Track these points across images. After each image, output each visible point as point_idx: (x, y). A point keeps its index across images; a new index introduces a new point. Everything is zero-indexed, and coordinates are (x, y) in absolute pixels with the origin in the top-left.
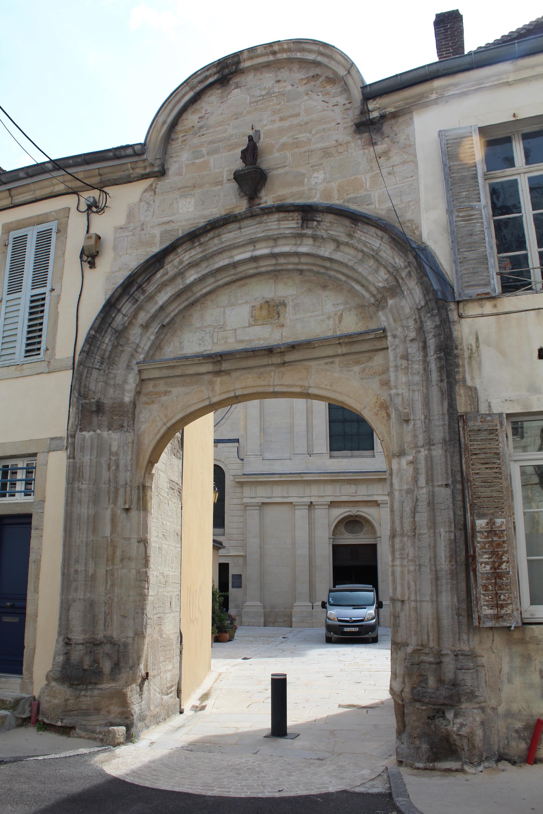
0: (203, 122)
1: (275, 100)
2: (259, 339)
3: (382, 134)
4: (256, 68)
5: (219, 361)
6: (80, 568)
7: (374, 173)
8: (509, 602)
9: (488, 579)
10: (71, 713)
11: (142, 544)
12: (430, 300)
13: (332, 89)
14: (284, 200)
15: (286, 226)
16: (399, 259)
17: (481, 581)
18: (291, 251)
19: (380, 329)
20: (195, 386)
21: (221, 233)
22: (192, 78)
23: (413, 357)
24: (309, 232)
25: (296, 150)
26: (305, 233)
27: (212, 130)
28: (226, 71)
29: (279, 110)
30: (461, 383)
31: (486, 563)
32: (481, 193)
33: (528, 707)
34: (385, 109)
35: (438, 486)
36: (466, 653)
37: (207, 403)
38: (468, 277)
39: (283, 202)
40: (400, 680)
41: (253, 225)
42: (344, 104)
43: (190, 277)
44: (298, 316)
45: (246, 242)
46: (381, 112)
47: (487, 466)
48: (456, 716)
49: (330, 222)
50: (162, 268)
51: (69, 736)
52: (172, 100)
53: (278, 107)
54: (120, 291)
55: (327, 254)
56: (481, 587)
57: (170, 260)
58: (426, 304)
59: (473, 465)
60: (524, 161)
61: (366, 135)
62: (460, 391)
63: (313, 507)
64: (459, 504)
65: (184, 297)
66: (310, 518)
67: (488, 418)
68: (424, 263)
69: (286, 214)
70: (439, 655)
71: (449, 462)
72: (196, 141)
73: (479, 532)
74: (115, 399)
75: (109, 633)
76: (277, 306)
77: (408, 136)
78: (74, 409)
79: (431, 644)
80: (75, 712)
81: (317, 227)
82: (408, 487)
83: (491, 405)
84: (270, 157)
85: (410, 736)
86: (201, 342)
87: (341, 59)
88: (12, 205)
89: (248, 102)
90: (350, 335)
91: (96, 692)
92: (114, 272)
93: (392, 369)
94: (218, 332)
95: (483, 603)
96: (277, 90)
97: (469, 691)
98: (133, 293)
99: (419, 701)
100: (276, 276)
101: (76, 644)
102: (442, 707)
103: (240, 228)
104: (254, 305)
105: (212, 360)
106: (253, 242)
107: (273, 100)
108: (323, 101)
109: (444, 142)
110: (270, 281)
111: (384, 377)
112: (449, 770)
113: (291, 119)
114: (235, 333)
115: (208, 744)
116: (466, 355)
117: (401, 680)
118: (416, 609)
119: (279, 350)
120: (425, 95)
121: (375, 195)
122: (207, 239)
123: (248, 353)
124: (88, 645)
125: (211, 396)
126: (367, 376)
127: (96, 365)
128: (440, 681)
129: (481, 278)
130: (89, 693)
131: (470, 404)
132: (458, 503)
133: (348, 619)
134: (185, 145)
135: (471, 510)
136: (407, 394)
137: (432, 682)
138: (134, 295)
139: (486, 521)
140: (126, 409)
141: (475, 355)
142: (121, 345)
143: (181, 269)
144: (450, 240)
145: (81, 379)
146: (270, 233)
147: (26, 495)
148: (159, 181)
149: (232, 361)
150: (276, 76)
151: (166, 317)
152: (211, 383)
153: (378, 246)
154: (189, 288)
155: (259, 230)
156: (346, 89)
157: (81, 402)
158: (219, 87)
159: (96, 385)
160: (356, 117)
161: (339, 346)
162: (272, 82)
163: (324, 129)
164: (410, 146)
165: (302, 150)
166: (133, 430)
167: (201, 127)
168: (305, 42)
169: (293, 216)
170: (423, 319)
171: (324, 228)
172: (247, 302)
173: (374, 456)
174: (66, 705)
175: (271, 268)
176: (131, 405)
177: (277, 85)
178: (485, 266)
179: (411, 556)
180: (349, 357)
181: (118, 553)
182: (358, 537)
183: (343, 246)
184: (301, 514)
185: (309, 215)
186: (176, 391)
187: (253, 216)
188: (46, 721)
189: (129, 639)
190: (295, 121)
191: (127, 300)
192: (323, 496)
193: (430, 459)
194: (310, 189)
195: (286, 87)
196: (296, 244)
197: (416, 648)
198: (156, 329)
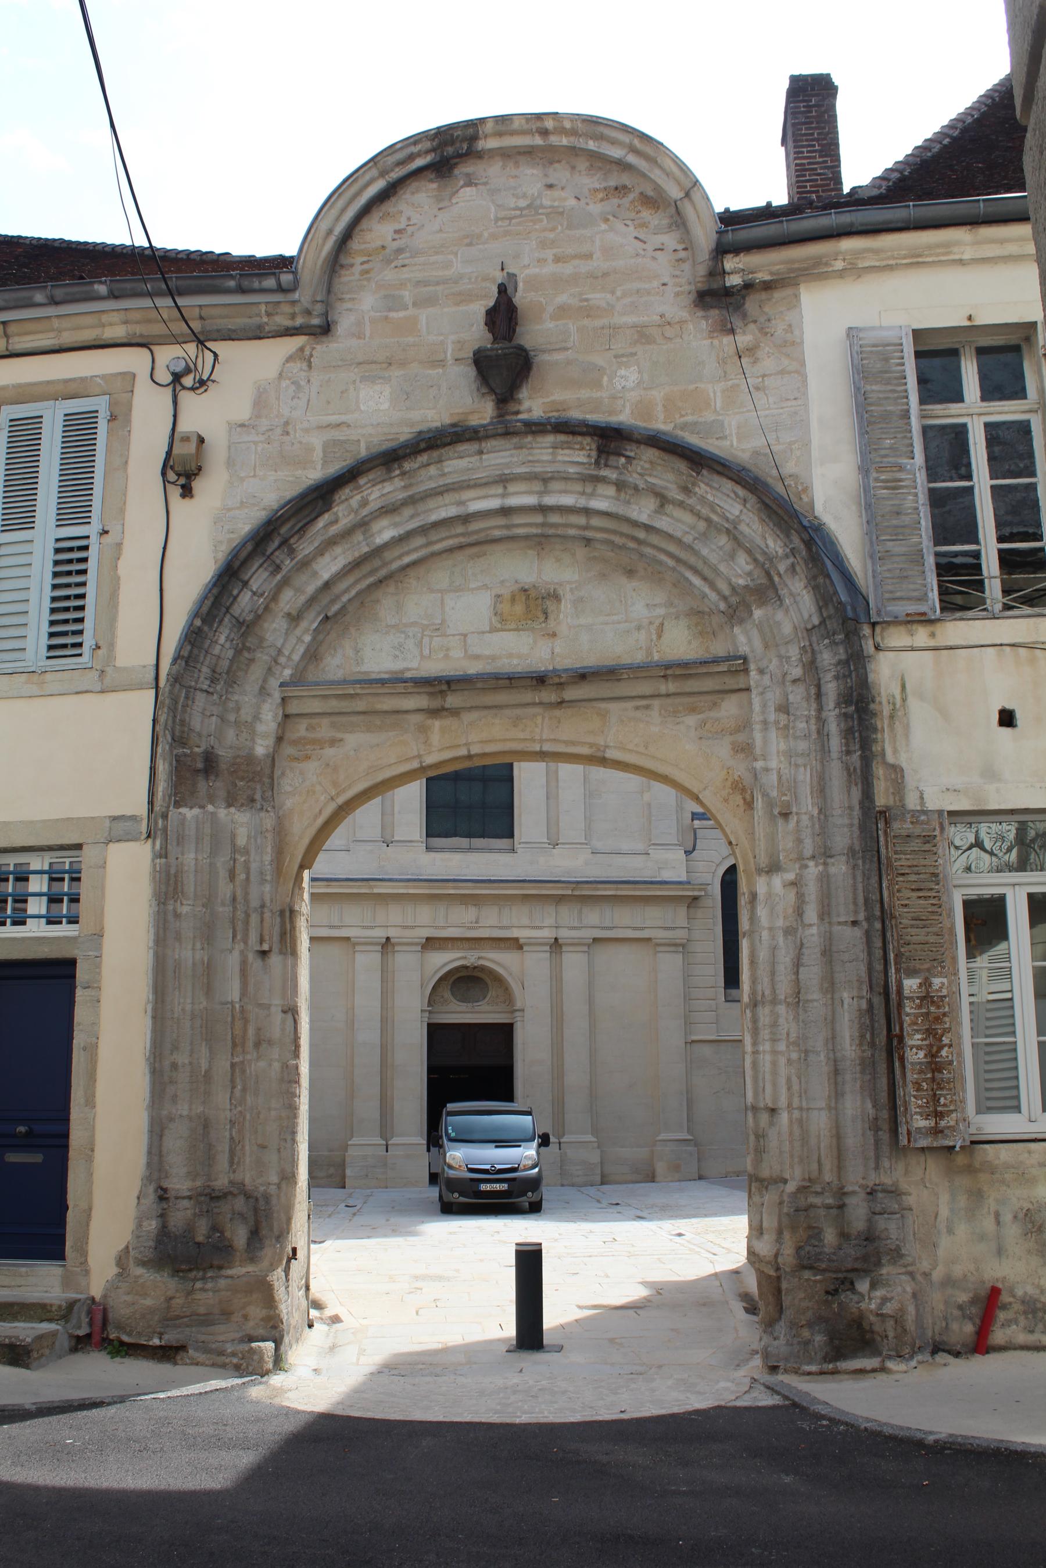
0: (403, 241)
1: (545, 221)
2: (510, 656)
3: (744, 316)
4: (506, 154)
5: (441, 692)
6: (182, 1058)
7: (730, 383)
8: (952, 1108)
9: (921, 1072)
10: (177, 1322)
11: (289, 1016)
12: (830, 617)
13: (655, 219)
14: (564, 410)
15: (567, 459)
16: (775, 541)
17: (911, 1076)
19: (740, 657)
20: (391, 734)
22: (385, 153)
23: (797, 709)
24: (613, 475)
25: (586, 322)
28: (450, 150)
30: (879, 758)
31: (919, 1048)
32: (915, 445)
33: (977, 1270)
34: (752, 273)
35: (839, 923)
36: (890, 1188)
37: (415, 765)
38: (893, 584)
40: (769, 1238)
41: (506, 450)
42: (675, 251)
43: (380, 532)
44: (582, 621)
45: (491, 480)
46: (746, 278)
47: (921, 894)
48: (873, 1286)
49: (651, 462)
51: (175, 1364)
54: (249, 547)
55: (644, 518)
56: (910, 1085)
57: (343, 497)
58: (823, 622)
59: (899, 891)
60: (978, 394)
61: (715, 313)
62: (879, 771)
63: (390, 948)
64: (878, 953)
65: (366, 568)
66: (384, 970)
67: (923, 818)
68: (823, 555)
69: (570, 438)
70: (842, 1193)
71: (860, 887)
72: (389, 275)
73: (908, 998)
74: (239, 749)
75: (238, 1177)
76: (543, 598)
77: (790, 326)
78: (167, 765)
79: (828, 1177)
80: (186, 1320)
81: (625, 467)
82: (788, 924)
83: (925, 796)
84: (538, 327)
85: (793, 1325)
86: (397, 653)
88: (7, 353)
91: (222, 1283)
92: (230, 510)
93: (757, 727)
94: (431, 637)
95: (914, 1110)
97: (893, 1247)
98: (272, 553)
99: (811, 1268)
100: (540, 544)
101: (177, 1198)
102: (850, 1275)
103: (481, 452)
104: (499, 593)
105: (431, 689)
106: (504, 480)
107: (541, 221)
108: (636, 238)
109: (856, 348)
110: (530, 552)
111: (741, 738)
112: (861, 1372)
113: (576, 262)
114: (465, 641)
115: (421, 1366)
116: (886, 712)
117: (774, 1237)
118: (800, 1121)
119: (557, 680)
120: (824, 260)
121: (732, 422)
122: (417, 465)
123: (500, 682)
124: (203, 1198)
125: (422, 753)
126: (710, 735)
127: (203, 683)
128: (844, 1235)
129: (912, 586)
130: (209, 1285)
131: (893, 793)
132: (877, 951)
133: (488, 1167)
134: (369, 280)
135: (896, 964)
136: (787, 771)
137: (830, 1236)
138: (273, 557)
139: (918, 981)
140: (259, 769)
141: (899, 713)
142: (249, 649)
144: (864, 519)
145: (176, 709)
146: (538, 469)
147: (49, 923)
148: (317, 343)
149: (466, 692)
150: (546, 175)
151: (333, 601)
152: (423, 729)
153: (737, 513)
154: (378, 551)
155: (515, 459)
156: (679, 222)
157: (175, 752)
158: (433, 176)
159: (202, 722)
161: (662, 679)
162: (539, 185)
163: (638, 291)
164: (793, 343)
165: (598, 323)
166: (274, 807)
167: (399, 251)
169: (581, 443)
170: (816, 648)
171: (639, 469)
172: (485, 587)
173: (513, 850)
174: (169, 1308)
175: (535, 531)
176: (269, 761)
177: (549, 192)
178: (920, 568)
179: (793, 1036)
180: (678, 700)
181: (251, 1032)
182: (477, 1009)
183: (671, 506)
184: (368, 961)
186: (353, 739)
187: (507, 434)
188: (125, 1338)
189: (272, 1187)
190: (584, 267)
191: (261, 566)
192: (413, 927)
193: (825, 879)
194: (614, 398)
195: (565, 199)
196: (583, 493)
197: (801, 1183)
198: (313, 621)
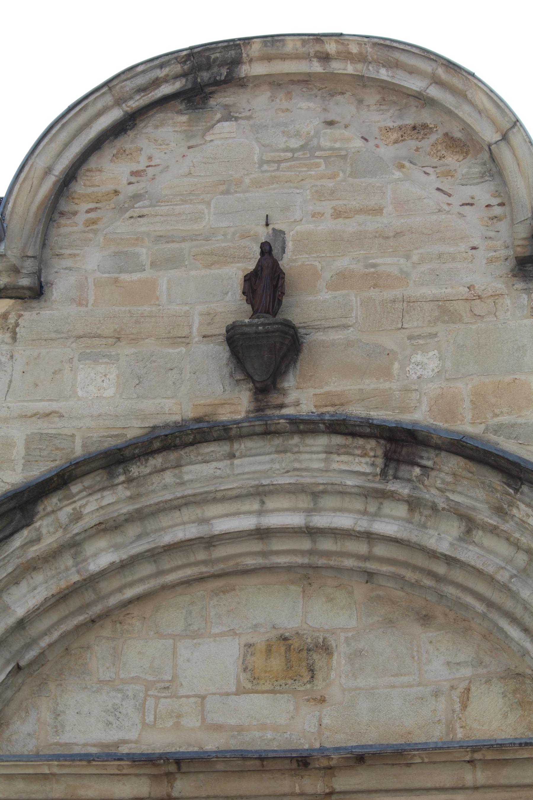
0: (142, 185)
1: (323, 166)
2: (263, 727)
5: (168, 774)
14: (342, 405)
15: (344, 467)
18: (358, 529)
21: (183, 462)
22: (123, 77)
25: (373, 293)
26: (393, 492)
27: (164, 209)
28: (205, 76)
29: (332, 192)
39: (340, 410)
41: (264, 454)
43: (95, 555)
44: (361, 682)
45: (244, 492)
49: (454, 475)
50: (28, 525)
52: (69, 120)
53: (330, 184)
55: (444, 548)
57: (49, 509)
65: (75, 603)
69: (349, 441)
76: (309, 650)
84: (311, 298)
86: (111, 719)
87: (489, 105)
89: (256, 159)
90: (501, 745)
94: (158, 698)
96: (328, 144)
100: (306, 577)
103: (232, 456)
104: (251, 641)
105: (154, 771)
107: (318, 165)
108: (438, 189)
110: (293, 588)
113: (360, 218)
114: (203, 705)
119: (325, 763)
122: (147, 470)
123: (248, 763)
143: (77, 534)
148: (26, 310)
149: (201, 776)
150: (325, 110)
151: (28, 646)
155: (277, 466)
160: (520, 242)
161: (468, 766)
163: (440, 256)
167: (136, 197)
168: (403, 50)
169: (363, 448)
171: (439, 484)
172: (233, 633)
175: (299, 560)
177: (329, 131)
183: (480, 533)
185: (404, 451)
194: (407, 390)
195: (349, 140)
196: (365, 513)
